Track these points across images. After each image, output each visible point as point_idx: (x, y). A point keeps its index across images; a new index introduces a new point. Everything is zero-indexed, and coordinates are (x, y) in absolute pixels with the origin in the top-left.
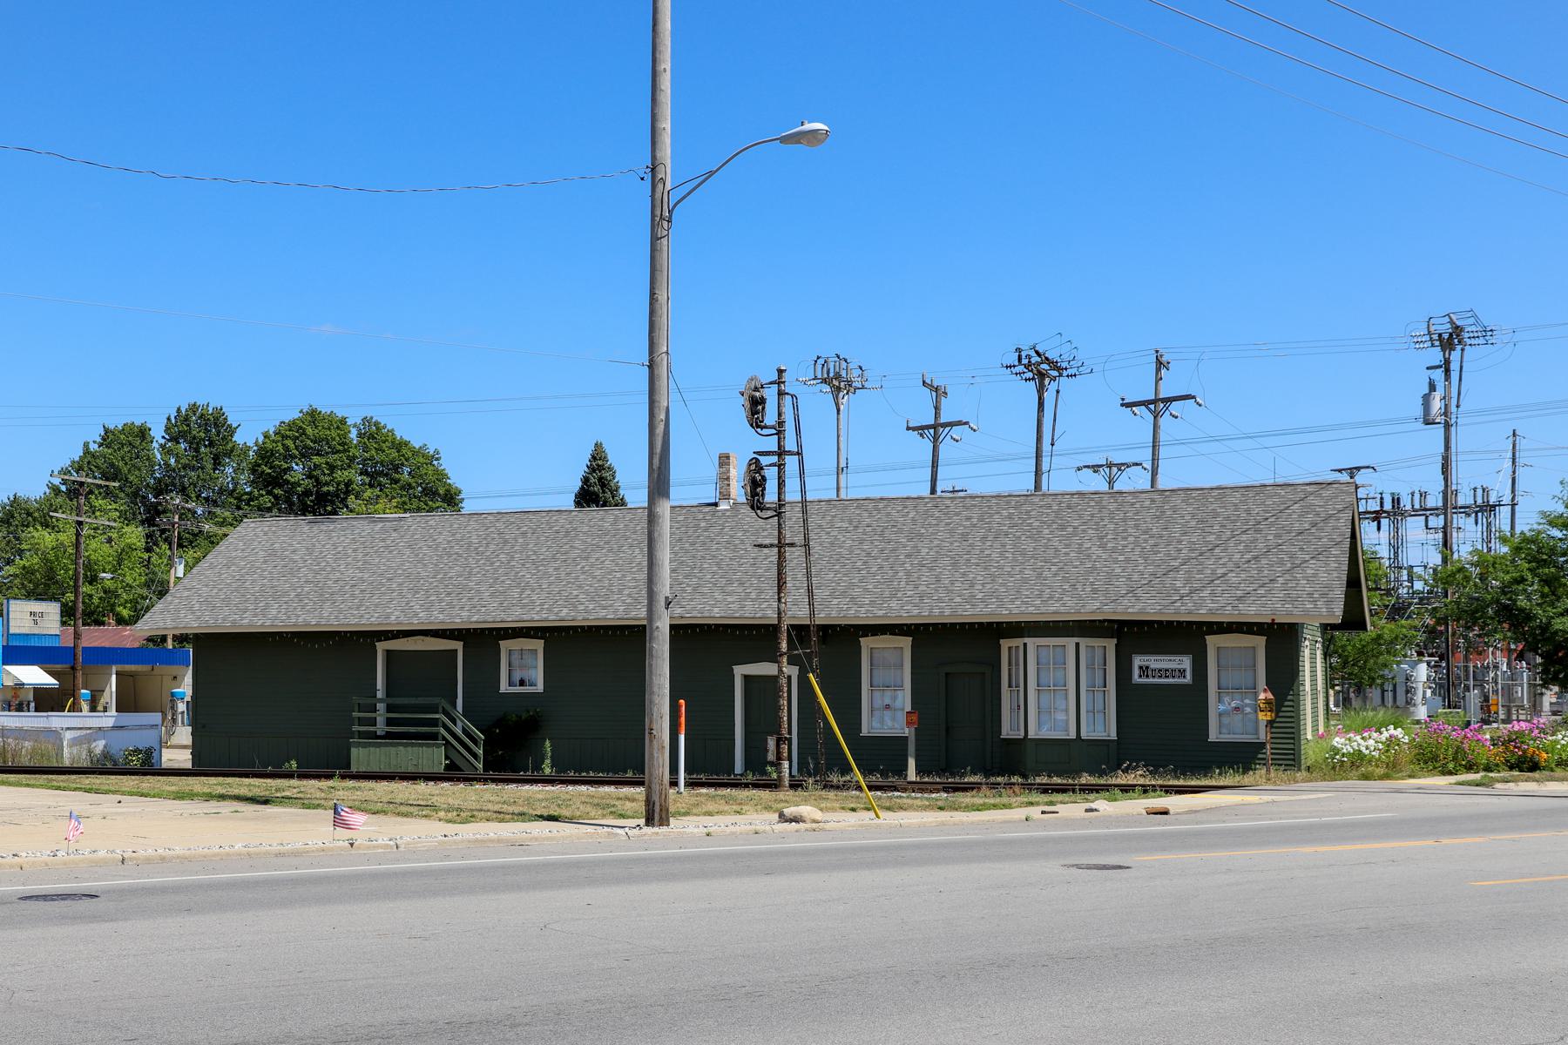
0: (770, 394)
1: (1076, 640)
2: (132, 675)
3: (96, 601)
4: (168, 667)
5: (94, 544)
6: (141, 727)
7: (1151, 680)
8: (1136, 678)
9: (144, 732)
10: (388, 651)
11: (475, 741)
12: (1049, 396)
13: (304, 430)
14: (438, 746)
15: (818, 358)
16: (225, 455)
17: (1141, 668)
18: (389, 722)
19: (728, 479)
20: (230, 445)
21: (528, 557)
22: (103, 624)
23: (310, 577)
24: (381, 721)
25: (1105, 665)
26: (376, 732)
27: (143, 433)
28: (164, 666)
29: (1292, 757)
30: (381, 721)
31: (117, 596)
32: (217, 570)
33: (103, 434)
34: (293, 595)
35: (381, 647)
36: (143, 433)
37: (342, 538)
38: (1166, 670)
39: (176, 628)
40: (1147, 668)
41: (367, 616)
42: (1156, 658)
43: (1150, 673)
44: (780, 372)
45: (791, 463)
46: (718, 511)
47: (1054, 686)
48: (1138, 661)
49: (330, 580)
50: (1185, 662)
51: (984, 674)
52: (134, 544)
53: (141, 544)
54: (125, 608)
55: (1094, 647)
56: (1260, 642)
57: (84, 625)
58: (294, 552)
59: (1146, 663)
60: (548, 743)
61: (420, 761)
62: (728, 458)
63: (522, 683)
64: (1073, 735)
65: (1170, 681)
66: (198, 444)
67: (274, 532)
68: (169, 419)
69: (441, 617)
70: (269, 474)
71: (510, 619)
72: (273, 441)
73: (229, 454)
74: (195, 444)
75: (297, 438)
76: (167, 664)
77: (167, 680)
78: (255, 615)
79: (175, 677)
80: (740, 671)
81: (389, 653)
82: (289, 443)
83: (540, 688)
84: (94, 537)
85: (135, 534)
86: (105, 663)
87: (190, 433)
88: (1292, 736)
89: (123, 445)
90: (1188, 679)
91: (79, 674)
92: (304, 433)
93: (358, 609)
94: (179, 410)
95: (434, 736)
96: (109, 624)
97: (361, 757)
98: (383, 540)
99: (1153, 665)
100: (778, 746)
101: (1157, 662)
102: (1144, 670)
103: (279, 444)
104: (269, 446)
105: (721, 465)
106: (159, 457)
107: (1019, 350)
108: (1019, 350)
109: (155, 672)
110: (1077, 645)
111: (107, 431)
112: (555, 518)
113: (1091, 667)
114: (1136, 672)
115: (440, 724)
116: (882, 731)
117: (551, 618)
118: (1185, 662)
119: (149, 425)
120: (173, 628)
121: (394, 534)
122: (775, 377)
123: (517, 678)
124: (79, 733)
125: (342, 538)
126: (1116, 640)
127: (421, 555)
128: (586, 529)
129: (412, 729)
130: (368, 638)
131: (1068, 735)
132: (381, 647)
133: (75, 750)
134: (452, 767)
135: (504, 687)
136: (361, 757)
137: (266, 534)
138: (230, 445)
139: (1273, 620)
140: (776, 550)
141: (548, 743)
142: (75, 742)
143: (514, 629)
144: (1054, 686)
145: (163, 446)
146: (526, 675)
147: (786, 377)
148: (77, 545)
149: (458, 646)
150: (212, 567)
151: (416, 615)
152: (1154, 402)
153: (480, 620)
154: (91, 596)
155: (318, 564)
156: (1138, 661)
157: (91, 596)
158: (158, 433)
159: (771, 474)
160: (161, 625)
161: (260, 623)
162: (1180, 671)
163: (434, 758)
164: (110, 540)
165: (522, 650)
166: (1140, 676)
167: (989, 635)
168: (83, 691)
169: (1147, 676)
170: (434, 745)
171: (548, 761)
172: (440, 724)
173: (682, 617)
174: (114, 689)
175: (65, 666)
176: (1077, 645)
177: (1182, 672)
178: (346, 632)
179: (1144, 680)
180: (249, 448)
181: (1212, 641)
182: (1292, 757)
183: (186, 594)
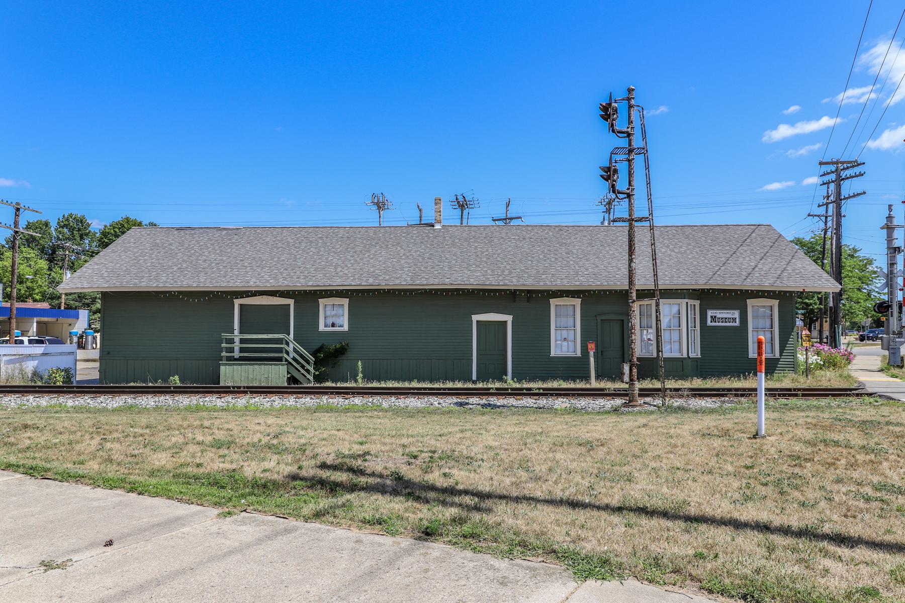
0: (621, 107)
1: (687, 300)
2: (45, 323)
3: (23, 292)
4: (67, 319)
5: (22, 267)
6: (61, 354)
7: (717, 324)
8: (709, 323)
9: (63, 357)
10: (241, 305)
11: (308, 362)
12: (465, 216)
13: (123, 225)
14: (282, 365)
15: (374, 194)
16: (85, 235)
17: (712, 317)
18: (242, 350)
19: (440, 212)
20: (87, 231)
21: (330, 250)
22: (26, 302)
23: (185, 258)
24: (237, 349)
25: (679, 314)
26: (234, 356)
27: (47, 224)
28: (65, 319)
29: (793, 366)
30: (237, 349)
31: (34, 290)
32: (117, 254)
33: (27, 224)
34: (175, 268)
35: (237, 302)
36: (47, 224)
37: (201, 238)
38: (725, 319)
39: (92, 287)
40: (715, 317)
41: (232, 281)
42: (720, 312)
43: (717, 320)
44: (630, 91)
45: (638, 161)
46: (435, 229)
47: (673, 327)
48: (710, 313)
49: (200, 260)
50: (736, 314)
51: (623, 320)
52: (43, 267)
53: (47, 267)
54: (37, 295)
55: (670, 304)
56: (775, 303)
57: (17, 302)
58: (171, 244)
59: (715, 314)
60: (360, 363)
61: (270, 375)
62: (440, 200)
63: (333, 325)
64: (685, 355)
65: (728, 324)
66: (73, 229)
67: (155, 234)
68: (59, 219)
69: (286, 282)
70: (107, 242)
71: (335, 284)
72: (109, 229)
73: (87, 235)
74: (72, 230)
75: (120, 228)
76: (66, 317)
77: (65, 326)
78: (151, 280)
79: (70, 324)
80: (476, 318)
81: (241, 306)
82: (117, 230)
83: (346, 328)
84: (22, 264)
85: (43, 264)
86: (30, 316)
87: (69, 225)
88: (793, 354)
89: (37, 228)
90: (737, 323)
91: (14, 321)
92: (123, 226)
93: (224, 277)
94: (64, 216)
95: (280, 359)
96: (29, 302)
97: (229, 374)
98: (230, 240)
99: (719, 316)
100: (631, 370)
101: (720, 314)
102: (714, 318)
103: (112, 230)
104: (107, 230)
105: (436, 204)
106: (54, 233)
107: (456, 195)
108: (456, 195)
109: (58, 322)
110: (687, 303)
111: (29, 223)
112: (337, 230)
113: (691, 314)
114: (709, 319)
115: (284, 351)
116: (568, 353)
117: (363, 284)
118: (736, 314)
119: (49, 221)
120: (89, 288)
121: (236, 237)
122: (626, 95)
123: (330, 322)
124: (13, 357)
125: (201, 238)
126: (699, 301)
127: (258, 248)
128: (359, 236)
129: (264, 355)
130: (229, 296)
131: (682, 355)
132: (237, 302)
133: (10, 367)
134: (292, 380)
135: (322, 328)
136: (229, 374)
137: (148, 235)
138: (87, 231)
139: (804, 290)
140: (627, 224)
141: (360, 363)
142: (9, 362)
143: (337, 291)
144: (673, 327)
145: (56, 230)
146: (338, 321)
147: (634, 94)
148: (13, 266)
149: (291, 302)
150: (113, 251)
151: (268, 281)
152: (505, 219)
153: (314, 285)
154: (20, 290)
155: (189, 251)
156: (710, 313)
157: (20, 290)
158: (53, 225)
159: (622, 168)
160: (79, 285)
161: (155, 285)
162: (733, 319)
163: (277, 374)
164: (30, 266)
165: (334, 305)
166: (711, 322)
167: (621, 298)
168: (16, 331)
169: (715, 322)
170: (279, 364)
171: (360, 375)
172: (284, 351)
173: (452, 284)
174: (35, 330)
175: (4, 318)
176: (687, 303)
177: (734, 320)
178: (218, 292)
179: (713, 324)
180: (96, 233)
181: (750, 302)
182: (793, 366)
183: (96, 267)
